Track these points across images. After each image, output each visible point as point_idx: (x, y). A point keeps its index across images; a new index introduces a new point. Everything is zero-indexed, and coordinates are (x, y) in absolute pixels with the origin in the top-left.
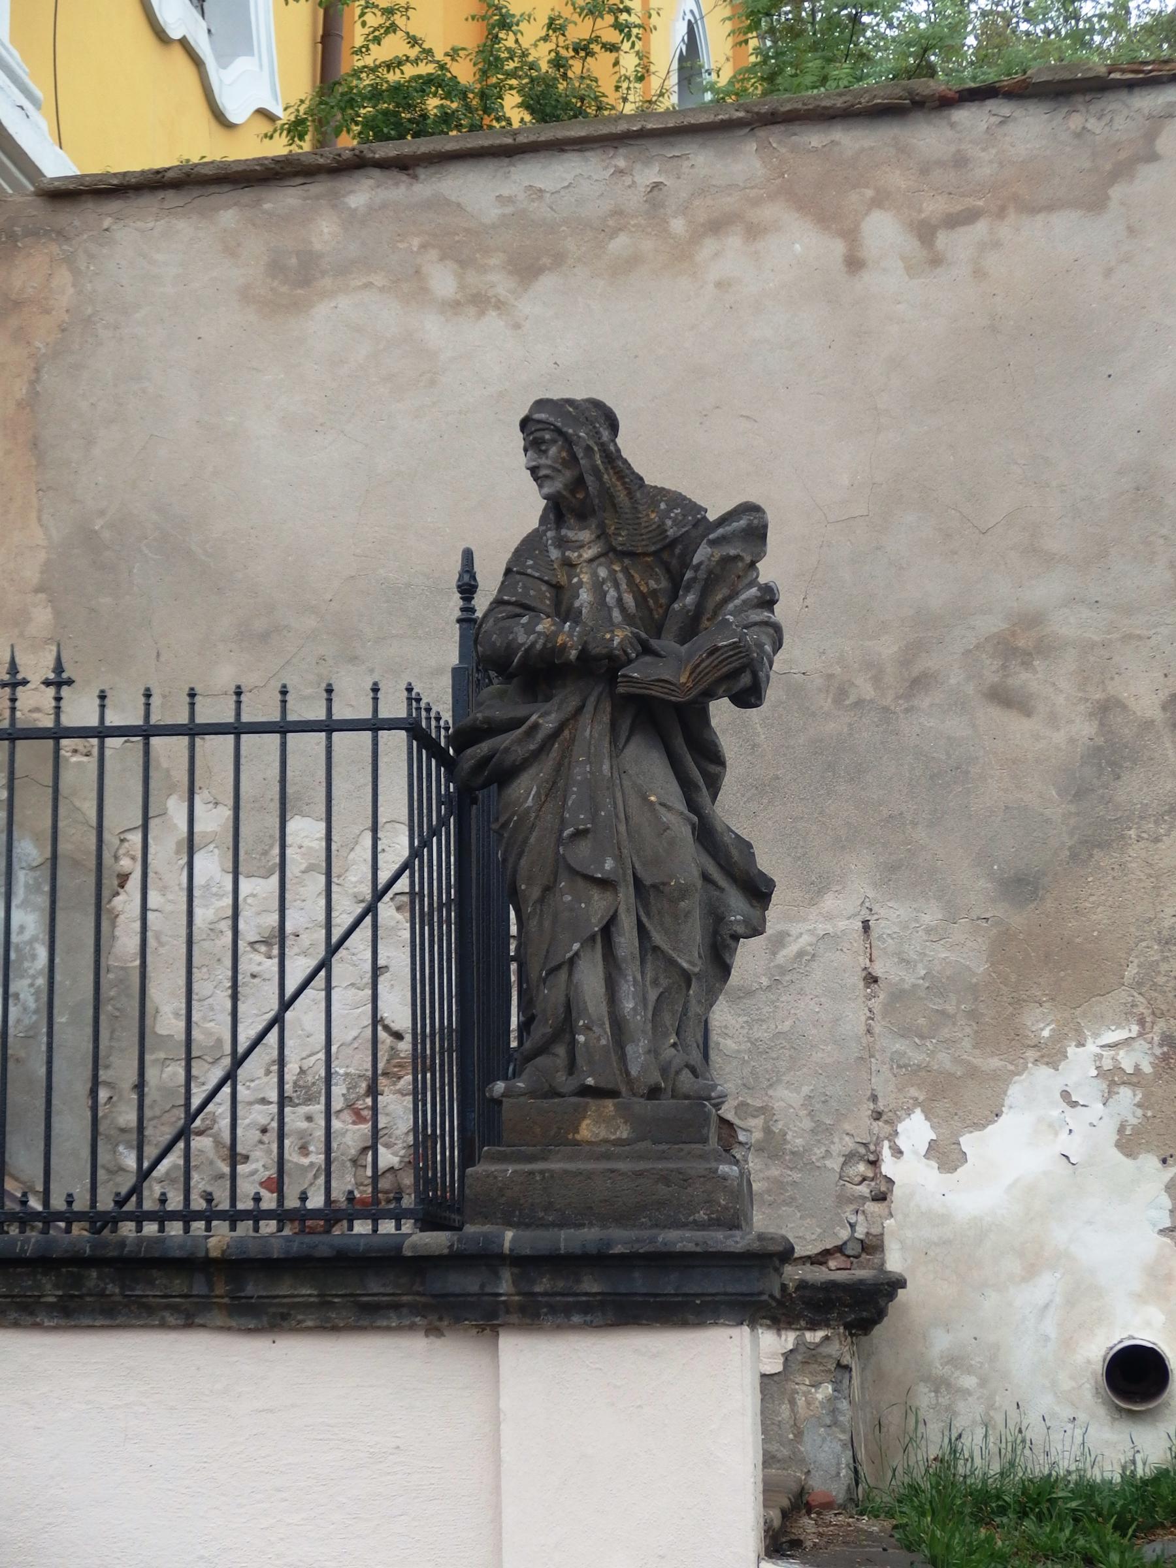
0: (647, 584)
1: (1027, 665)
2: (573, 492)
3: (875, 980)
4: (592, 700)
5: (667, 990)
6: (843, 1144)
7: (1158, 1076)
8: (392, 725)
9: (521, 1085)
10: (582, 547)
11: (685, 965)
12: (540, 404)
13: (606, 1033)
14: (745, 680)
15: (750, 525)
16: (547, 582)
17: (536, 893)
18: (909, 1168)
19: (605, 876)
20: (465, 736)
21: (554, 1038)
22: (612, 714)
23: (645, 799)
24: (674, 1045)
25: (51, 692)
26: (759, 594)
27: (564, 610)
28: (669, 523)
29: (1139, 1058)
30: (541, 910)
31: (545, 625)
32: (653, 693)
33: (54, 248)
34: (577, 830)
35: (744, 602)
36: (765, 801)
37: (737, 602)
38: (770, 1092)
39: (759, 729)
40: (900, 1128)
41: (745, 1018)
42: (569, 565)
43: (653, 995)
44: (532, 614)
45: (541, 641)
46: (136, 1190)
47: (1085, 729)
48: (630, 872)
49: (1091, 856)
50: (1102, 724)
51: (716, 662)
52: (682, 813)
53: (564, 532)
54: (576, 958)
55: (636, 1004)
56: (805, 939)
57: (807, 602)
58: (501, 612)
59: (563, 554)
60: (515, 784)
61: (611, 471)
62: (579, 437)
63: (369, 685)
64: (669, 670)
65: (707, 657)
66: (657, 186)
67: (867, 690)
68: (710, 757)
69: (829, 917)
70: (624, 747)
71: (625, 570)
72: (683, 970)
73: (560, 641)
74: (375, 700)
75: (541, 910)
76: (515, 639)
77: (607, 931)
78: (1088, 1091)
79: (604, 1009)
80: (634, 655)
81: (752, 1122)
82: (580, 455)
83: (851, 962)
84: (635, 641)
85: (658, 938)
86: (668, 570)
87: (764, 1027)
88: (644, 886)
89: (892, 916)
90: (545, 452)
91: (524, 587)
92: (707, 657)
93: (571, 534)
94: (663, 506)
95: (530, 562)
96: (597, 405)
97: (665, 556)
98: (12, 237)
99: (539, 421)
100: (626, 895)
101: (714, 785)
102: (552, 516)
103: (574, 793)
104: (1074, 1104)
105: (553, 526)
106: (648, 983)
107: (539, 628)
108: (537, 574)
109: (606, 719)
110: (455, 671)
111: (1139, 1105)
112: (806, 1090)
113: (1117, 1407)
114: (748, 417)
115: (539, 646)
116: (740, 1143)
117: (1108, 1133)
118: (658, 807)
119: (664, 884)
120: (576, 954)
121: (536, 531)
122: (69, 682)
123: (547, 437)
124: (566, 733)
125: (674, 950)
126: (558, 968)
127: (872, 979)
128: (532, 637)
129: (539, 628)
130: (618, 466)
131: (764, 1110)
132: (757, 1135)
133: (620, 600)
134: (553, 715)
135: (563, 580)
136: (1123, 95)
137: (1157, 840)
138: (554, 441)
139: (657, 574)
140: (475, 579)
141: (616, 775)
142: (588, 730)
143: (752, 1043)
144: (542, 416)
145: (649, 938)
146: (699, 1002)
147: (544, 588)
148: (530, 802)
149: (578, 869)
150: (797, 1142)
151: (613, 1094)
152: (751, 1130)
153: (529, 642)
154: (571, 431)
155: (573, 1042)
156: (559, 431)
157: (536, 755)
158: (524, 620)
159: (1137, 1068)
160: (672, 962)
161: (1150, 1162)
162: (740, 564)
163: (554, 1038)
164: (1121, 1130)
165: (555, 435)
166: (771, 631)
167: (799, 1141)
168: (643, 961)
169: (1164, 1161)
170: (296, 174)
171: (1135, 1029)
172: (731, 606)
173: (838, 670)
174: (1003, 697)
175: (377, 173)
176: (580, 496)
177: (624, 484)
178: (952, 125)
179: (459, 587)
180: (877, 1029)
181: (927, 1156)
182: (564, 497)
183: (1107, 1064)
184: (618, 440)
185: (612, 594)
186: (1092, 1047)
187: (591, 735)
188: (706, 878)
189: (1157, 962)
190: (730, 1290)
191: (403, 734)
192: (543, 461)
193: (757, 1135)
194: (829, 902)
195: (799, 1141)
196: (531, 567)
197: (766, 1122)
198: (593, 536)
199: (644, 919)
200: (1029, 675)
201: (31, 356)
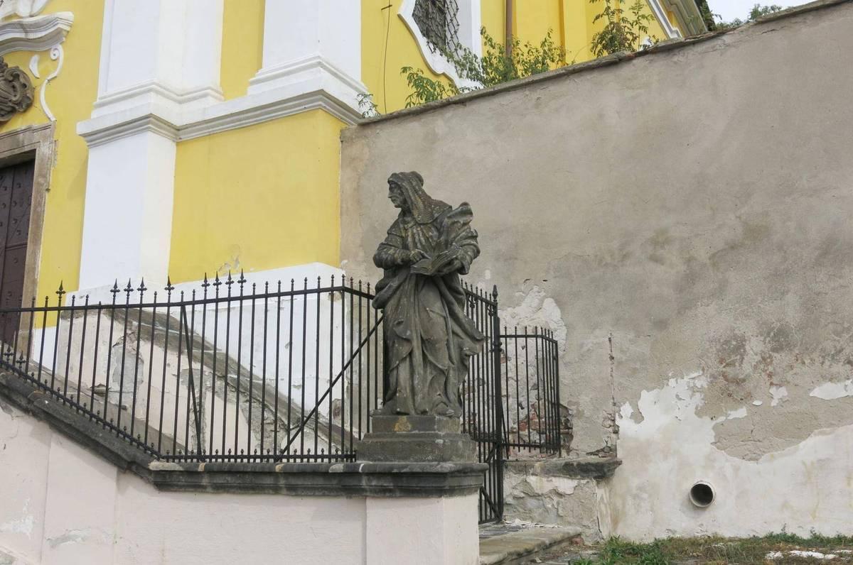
1: (662, 247)
3: (613, 358)
6: (603, 414)
7: (709, 389)
11: (441, 367)
15: (466, 211)
18: (625, 424)
23: (425, 308)
25: (113, 293)
27: (405, 247)
29: (702, 382)
33: (364, 141)
37: (459, 237)
40: (622, 409)
43: (430, 378)
46: (287, 448)
47: (682, 268)
49: (685, 312)
50: (688, 266)
56: (591, 345)
63: (317, 278)
66: (538, 98)
67: (608, 259)
69: (596, 337)
71: (421, 229)
77: (411, 354)
78: (685, 394)
80: (418, 259)
81: (573, 407)
82: (404, 191)
83: (606, 352)
85: (430, 358)
89: (618, 336)
98: (352, 139)
100: (416, 343)
104: (680, 399)
111: (703, 399)
112: (590, 396)
113: (694, 505)
115: (389, 259)
117: (692, 409)
120: (398, 364)
122: (146, 289)
126: (393, 369)
127: (612, 358)
132: (575, 412)
133: (420, 240)
135: (404, 235)
136: (691, 47)
137: (708, 306)
138: (395, 187)
150: (587, 413)
152: (573, 410)
158: (385, 250)
159: (702, 386)
160: (435, 367)
161: (707, 419)
162: (459, 224)
164: (697, 408)
169: (712, 419)
170: (431, 109)
171: (701, 372)
173: (599, 253)
174: (656, 259)
175: (454, 106)
178: (634, 65)
180: (614, 375)
181: (630, 418)
183: (692, 385)
185: (417, 237)
186: (686, 379)
189: (708, 349)
190: (434, 485)
193: (575, 412)
194: (597, 332)
199: (425, 351)
200: (662, 251)
201: (358, 175)
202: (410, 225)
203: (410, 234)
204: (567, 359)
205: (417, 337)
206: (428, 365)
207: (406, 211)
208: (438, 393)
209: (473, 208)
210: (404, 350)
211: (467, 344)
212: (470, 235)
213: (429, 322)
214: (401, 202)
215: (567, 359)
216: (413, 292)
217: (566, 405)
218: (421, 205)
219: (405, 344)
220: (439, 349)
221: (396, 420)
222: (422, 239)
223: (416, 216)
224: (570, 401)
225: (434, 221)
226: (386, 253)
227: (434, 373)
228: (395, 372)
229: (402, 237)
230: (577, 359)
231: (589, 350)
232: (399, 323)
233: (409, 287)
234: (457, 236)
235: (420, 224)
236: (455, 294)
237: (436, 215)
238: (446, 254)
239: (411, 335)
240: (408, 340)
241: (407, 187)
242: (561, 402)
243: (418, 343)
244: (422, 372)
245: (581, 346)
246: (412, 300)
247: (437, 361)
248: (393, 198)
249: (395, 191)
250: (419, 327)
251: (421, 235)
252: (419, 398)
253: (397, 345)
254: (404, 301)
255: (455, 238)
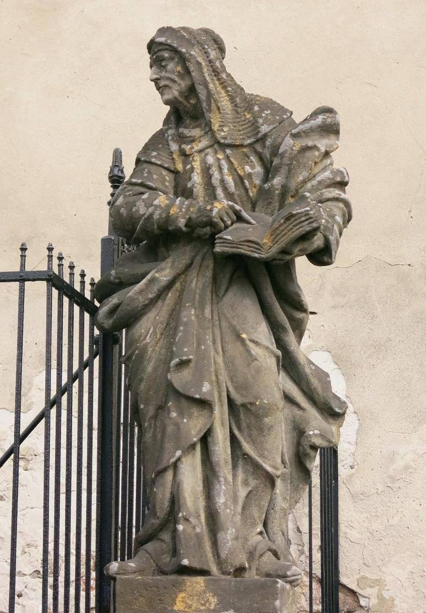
0: (243, 168)
2: (187, 98)
4: (198, 258)
5: (256, 488)
8: (35, 277)
9: (132, 565)
10: (193, 141)
11: (269, 469)
12: (162, 31)
13: (200, 523)
14: (318, 242)
16: (167, 169)
17: (151, 411)
19: (202, 397)
20: (103, 290)
21: (162, 527)
22: (214, 270)
23: (238, 336)
24: (261, 533)
26: (331, 176)
27: (182, 190)
28: (260, 121)
30: (155, 425)
31: (161, 200)
32: (243, 251)
34: (181, 360)
35: (320, 182)
36: (381, 357)
37: (314, 182)
38: (383, 569)
39: (377, 305)
41: (365, 515)
42: (185, 155)
43: (243, 493)
44: (151, 191)
45: (158, 212)
48: (225, 394)
51: (291, 226)
52: (267, 348)
53: (181, 130)
54: (179, 463)
55: (227, 500)
57: (412, 214)
58: (129, 191)
59: (180, 147)
60: (138, 325)
61: (217, 82)
62: (191, 55)
64: (256, 235)
65: (285, 222)
68: (294, 304)
70: (223, 296)
71: (227, 158)
72: (267, 473)
73: (172, 212)
74: (23, 257)
75: (155, 425)
76: (137, 211)
77: (206, 440)
79: (202, 503)
80: (229, 222)
82: (192, 68)
84: (231, 212)
85: (247, 447)
86: (261, 158)
87: (380, 521)
88: (236, 405)
90: (165, 67)
91: (149, 172)
92: (285, 222)
93: (186, 132)
94: (256, 108)
95: (154, 154)
96: (207, 32)
97: (258, 147)
99: (161, 44)
100: (220, 412)
101: (299, 328)
102: (172, 118)
103: (181, 331)
105: (173, 125)
106: (239, 483)
107: (156, 202)
108: (159, 163)
109: (209, 273)
110: (105, 242)
114: (370, 84)
116: (361, 607)
118: (248, 342)
119: (251, 404)
120: (179, 459)
121: (161, 130)
123: (166, 55)
124: (178, 285)
125: (260, 457)
126: (165, 470)
128: (151, 209)
129: (156, 202)
130: (223, 78)
131: (378, 583)
133: (222, 181)
134: (168, 271)
135: (180, 167)
138: (172, 59)
139: (252, 162)
140: (122, 172)
141: (216, 318)
142: (194, 283)
143: (370, 533)
144: (162, 39)
145: (240, 447)
146: (285, 499)
147: (164, 173)
148: (148, 340)
149: (180, 390)
151: (203, 572)
153: (148, 214)
154: (184, 50)
155: (175, 530)
156: (175, 51)
157: (153, 302)
158: (145, 196)
160: (257, 467)
163: (162, 527)
165: (173, 55)
166: (341, 205)
167: (404, 605)
168: (235, 467)
172: (309, 185)
176: (193, 101)
177: (227, 92)
179: (110, 178)
182: (180, 102)
184: (225, 62)
185: (216, 175)
187: (196, 286)
188: (288, 399)
191: (45, 283)
192: (163, 74)
193: (374, 601)
195: (404, 605)
196: (155, 157)
197: (379, 590)
198: (203, 132)
199: (236, 432)
202: (198, 146)
203: (197, 165)
204: (358, 485)
205: (220, 397)
206: (240, 463)
207: (186, 112)
208: (259, 530)
209: (343, 120)
210: (194, 426)
211: (314, 423)
212: (338, 179)
213: (249, 365)
214: (181, 93)
215: (358, 485)
216: (209, 289)
217: (353, 587)
218: (225, 103)
219: (195, 411)
220: (270, 428)
221: (178, 587)
222: (229, 180)
223: (216, 127)
224: (363, 578)
225: (257, 141)
226: (148, 204)
227: (253, 483)
228: (169, 475)
229: (175, 172)
230: (381, 488)
231: (407, 468)
232: (183, 364)
233: (198, 282)
234: (309, 180)
235: (223, 146)
236: (288, 309)
237: (264, 129)
238: (306, 214)
239: (211, 393)
240: (204, 404)
241: (200, 59)
242: (344, 580)
243: (222, 413)
244: (230, 478)
245: (391, 458)
246: (207, 311)
247: (261, 456)
248: (162, 83)
249: (171, 66)
250: (224, 377)
251: (226, 171)
252: (228, 537)
253: (174, 415)
254: (189, 314)
255: (304, 182)
